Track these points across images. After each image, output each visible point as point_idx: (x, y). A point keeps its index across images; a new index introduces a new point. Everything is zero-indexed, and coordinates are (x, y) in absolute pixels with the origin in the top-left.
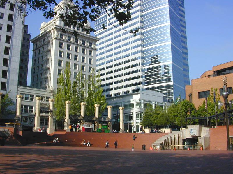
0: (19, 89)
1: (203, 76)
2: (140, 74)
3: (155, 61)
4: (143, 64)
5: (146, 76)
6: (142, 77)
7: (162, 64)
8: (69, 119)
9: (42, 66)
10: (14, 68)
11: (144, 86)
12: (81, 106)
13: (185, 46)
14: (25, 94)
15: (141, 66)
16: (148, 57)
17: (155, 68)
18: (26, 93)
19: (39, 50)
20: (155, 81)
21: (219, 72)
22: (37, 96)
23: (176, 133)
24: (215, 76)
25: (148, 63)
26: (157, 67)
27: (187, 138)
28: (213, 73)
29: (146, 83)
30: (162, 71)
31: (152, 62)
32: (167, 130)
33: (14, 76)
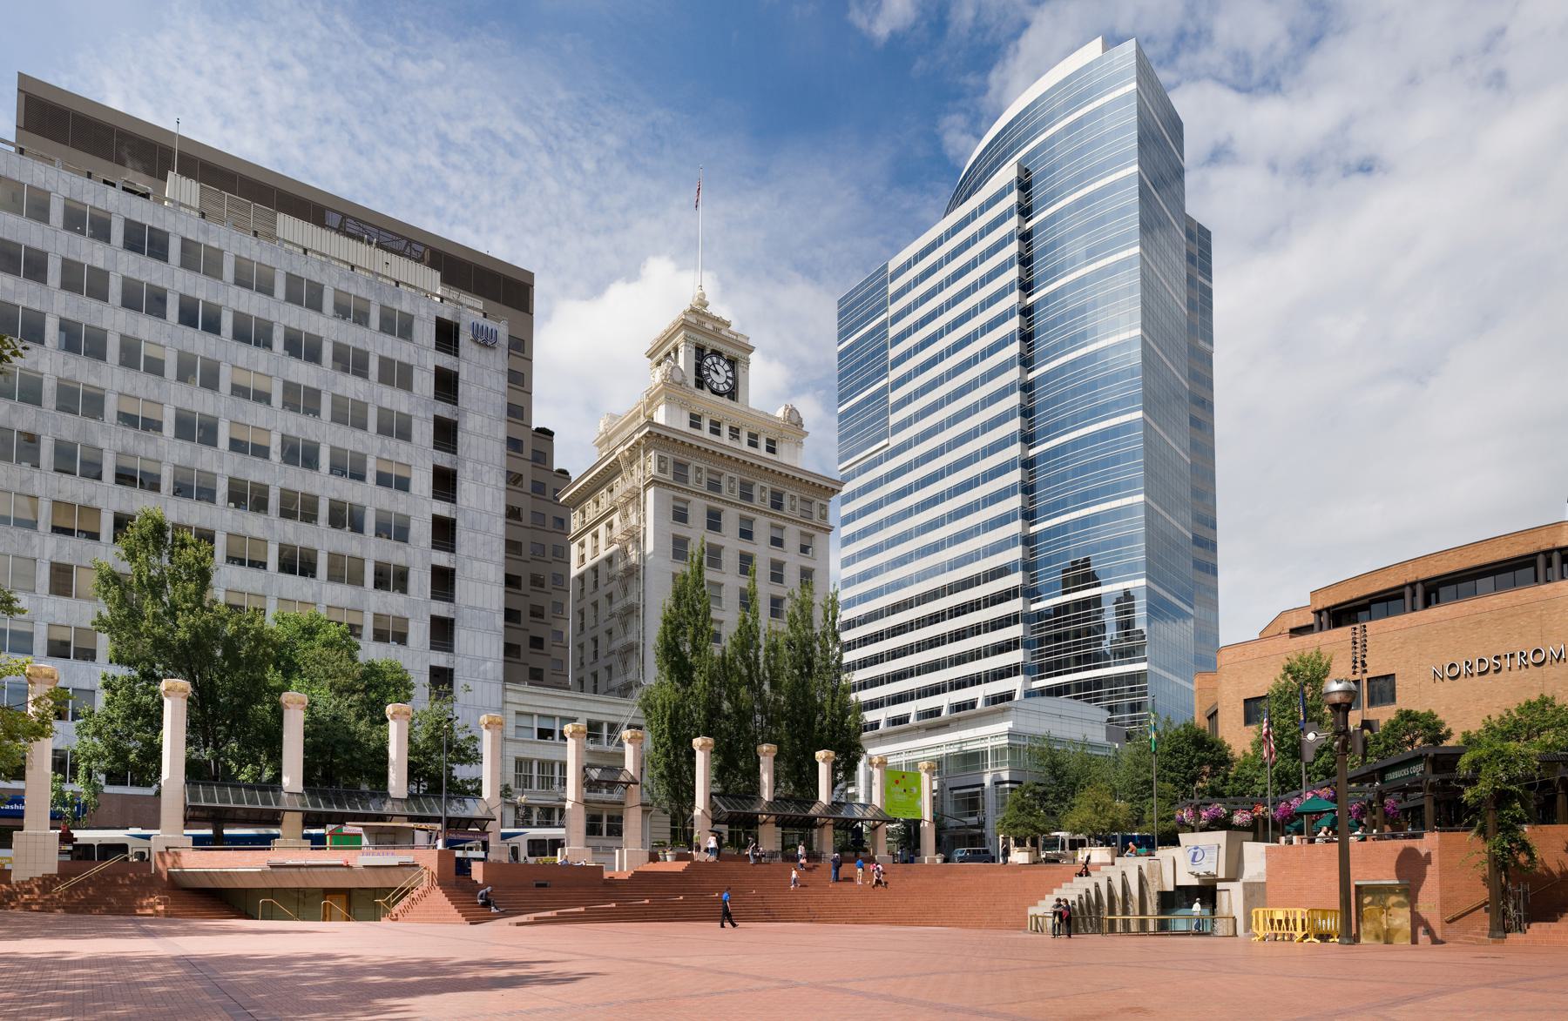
0: (511, 696)
1: (1265, 635)
2: (1016, 631)
3: (1076, 580)
4: (1030, 593)
5: (1041, 642)
6: (1027, 645)
7: (1109, 589)
8: (710, 814)
9: (611, 603)
10: (483, 609)
11: (1034, 680)
12: (694, 753)
13: (1207, 559)
14: (540, 715)
15: (1020, 599)
16: (1048, 561)
17: (1078, 605)
18: (541, 711)
19: (596, 536)
20: (1078, 660)
21: (1341, 614)
22: (629, 727)
23: (1131, 865)
24: (1321, 629)
25: (1049, 587)
26: (1086, 603)
27: (1178, 888)
28: (1311, 619)
29: (1041, 668)
30: (1110, 618)
31: (1065, 582)
32: (1099, 854)
33: (480, 645)
